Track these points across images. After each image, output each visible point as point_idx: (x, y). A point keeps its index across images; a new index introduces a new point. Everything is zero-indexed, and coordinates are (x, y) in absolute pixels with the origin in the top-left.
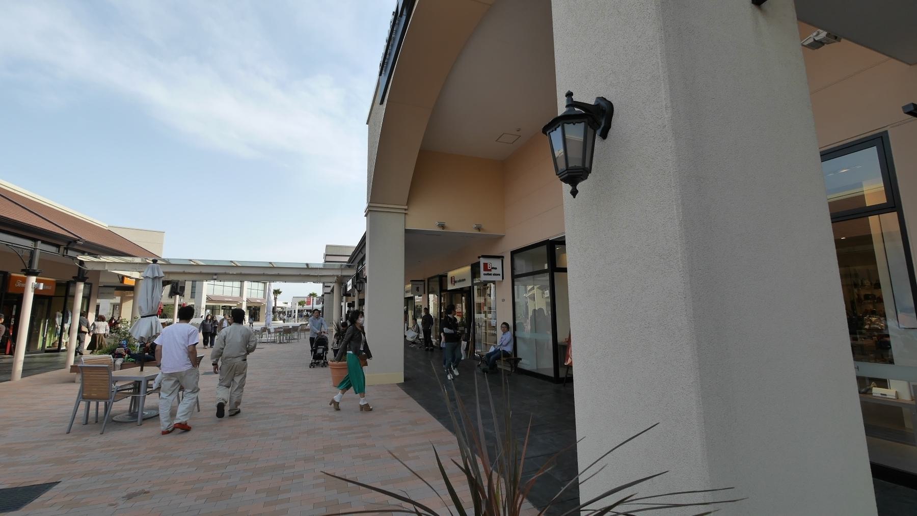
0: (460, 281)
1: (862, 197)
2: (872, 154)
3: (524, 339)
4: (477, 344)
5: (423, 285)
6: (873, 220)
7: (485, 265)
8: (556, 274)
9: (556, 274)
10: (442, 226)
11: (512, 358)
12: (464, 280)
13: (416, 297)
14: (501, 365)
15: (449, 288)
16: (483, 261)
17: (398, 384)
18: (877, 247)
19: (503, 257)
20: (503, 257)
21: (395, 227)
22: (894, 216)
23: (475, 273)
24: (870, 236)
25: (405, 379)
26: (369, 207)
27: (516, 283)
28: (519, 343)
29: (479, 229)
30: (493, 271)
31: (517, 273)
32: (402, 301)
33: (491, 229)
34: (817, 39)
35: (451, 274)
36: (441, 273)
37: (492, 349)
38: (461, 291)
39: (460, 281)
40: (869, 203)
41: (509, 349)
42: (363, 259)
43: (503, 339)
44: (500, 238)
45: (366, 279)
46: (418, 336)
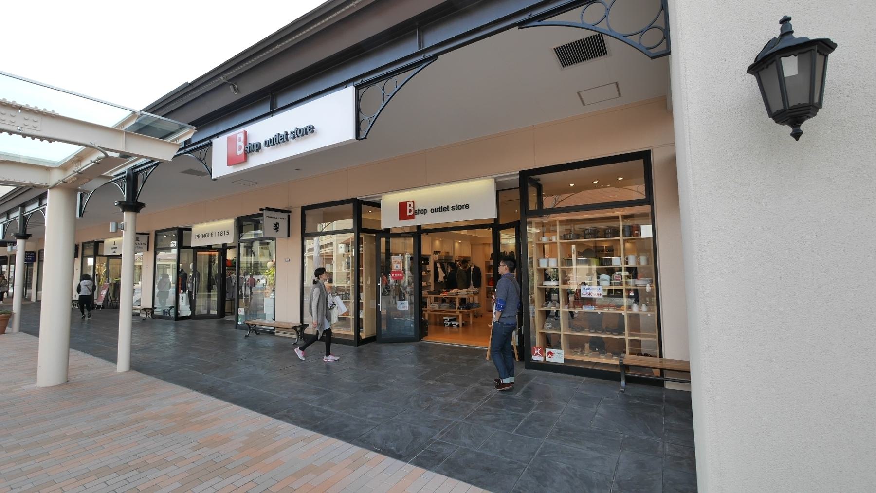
0: (456, 208)
20: (290, 212)
36: (97, 239)
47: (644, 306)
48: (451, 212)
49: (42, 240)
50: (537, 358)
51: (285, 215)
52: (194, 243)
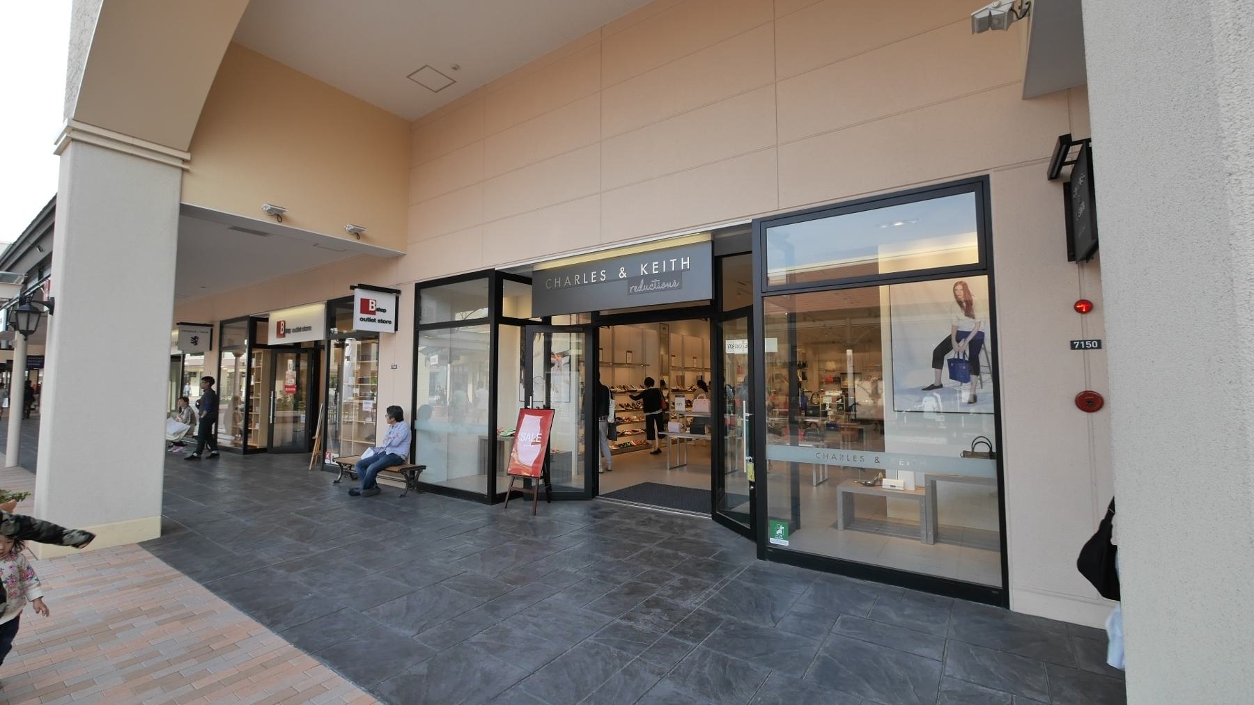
0: (298, 330)
1: (876, 265)
2: (970, 198)
3: (429, 434)
4: (330, 443)
5: (216, 335)
6: (883, 290)
7: (365, 303)
8: (501, 327)
9: (501, 327)
10: (278, 215)
11: (408, 467)
12: (308, 329)
13: (188, 356)
14: (388, 481)
15: (270, 343)
16: (359, 295)
17: (145, 545)
18: (884, 320)
19: (398, 292)
20: (398, 292)
21: (150, 203)
22: (984, 279)
23: (338, 311)
24: (878, 309)
25: (165, 530)
26: (70, 129)
27: (421, 341)
28: (419, 437)
29: (357, 234)
30: (379, 315)
31: (423, 322)
32: (168, 360)
33: (380, 238)
34: (994, 13)
35: (275, 317)
36: (255, 312)
37: (368, 454)
38: (296, 348)
39: (298, 330)
40: (882, 270)
41: (403, 451)
42: (45, 263)
43: (388, 437)
44: (396, 258)
45: (51, 304)
46: (189, 433)
47: (545, 432)
48: (377, 324)
49: (42, 342)
50: (778, 539)
51: (392, 299)
52: (273, 340)
